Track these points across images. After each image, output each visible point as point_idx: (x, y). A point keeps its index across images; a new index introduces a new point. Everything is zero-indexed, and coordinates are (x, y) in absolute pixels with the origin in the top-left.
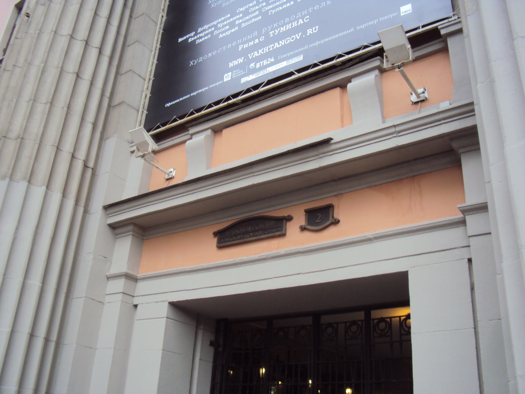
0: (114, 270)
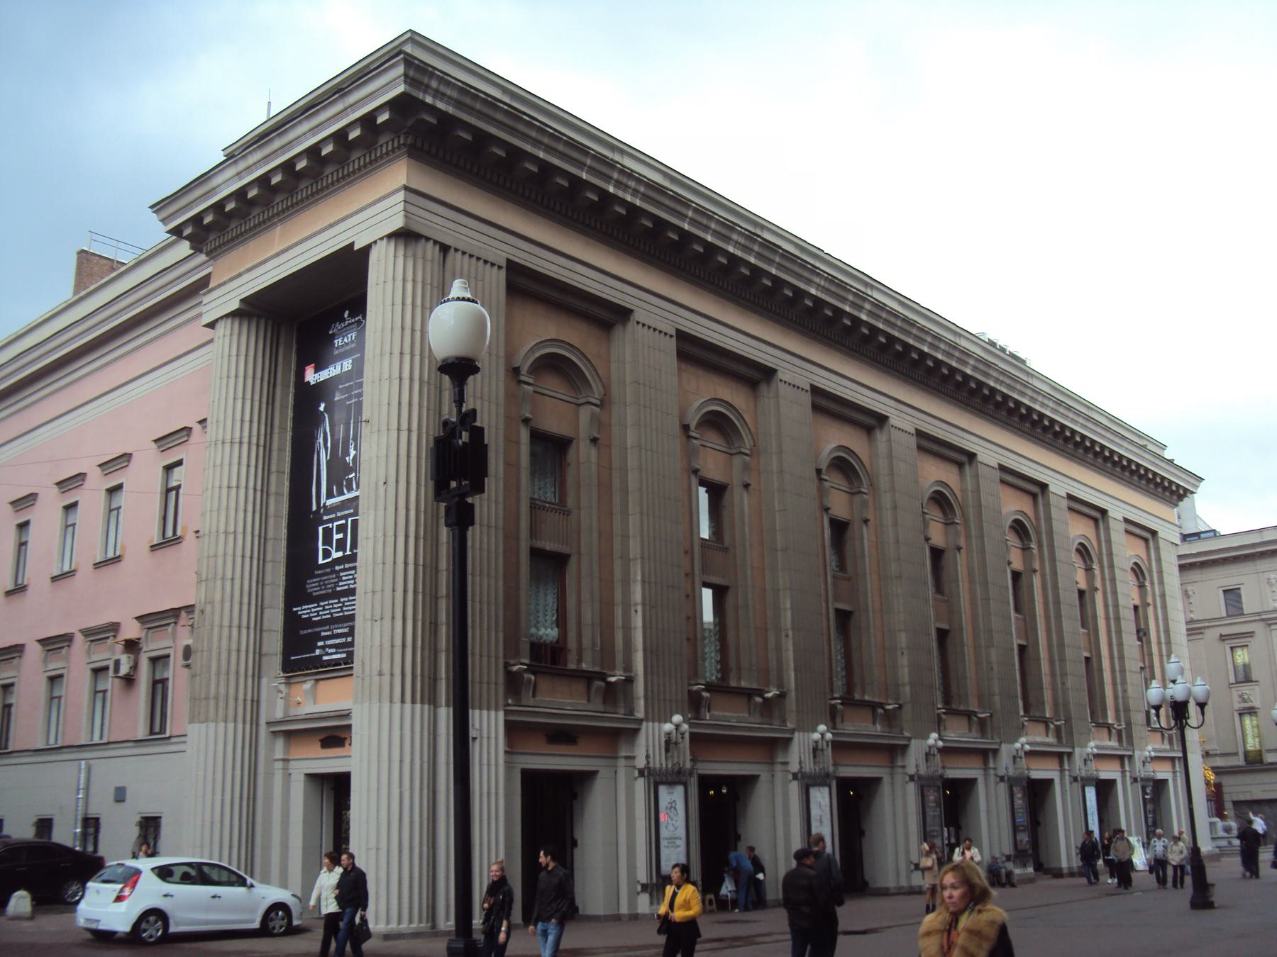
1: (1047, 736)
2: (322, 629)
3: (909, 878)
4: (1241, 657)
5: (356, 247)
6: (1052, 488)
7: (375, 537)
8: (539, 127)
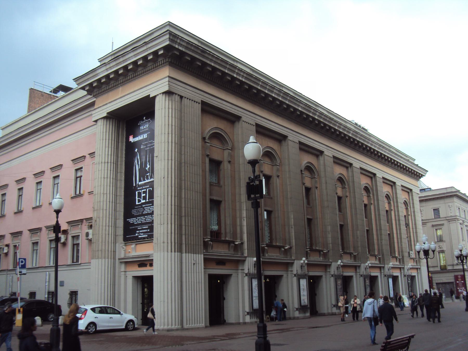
0: (122, 270)
1: (376, 261)
2: (138, 227)
3: (332, 310)
4: (439, 232)
5: (151, 96)
6: (377, 175)
7: (161, 196)
8: (314, 109)
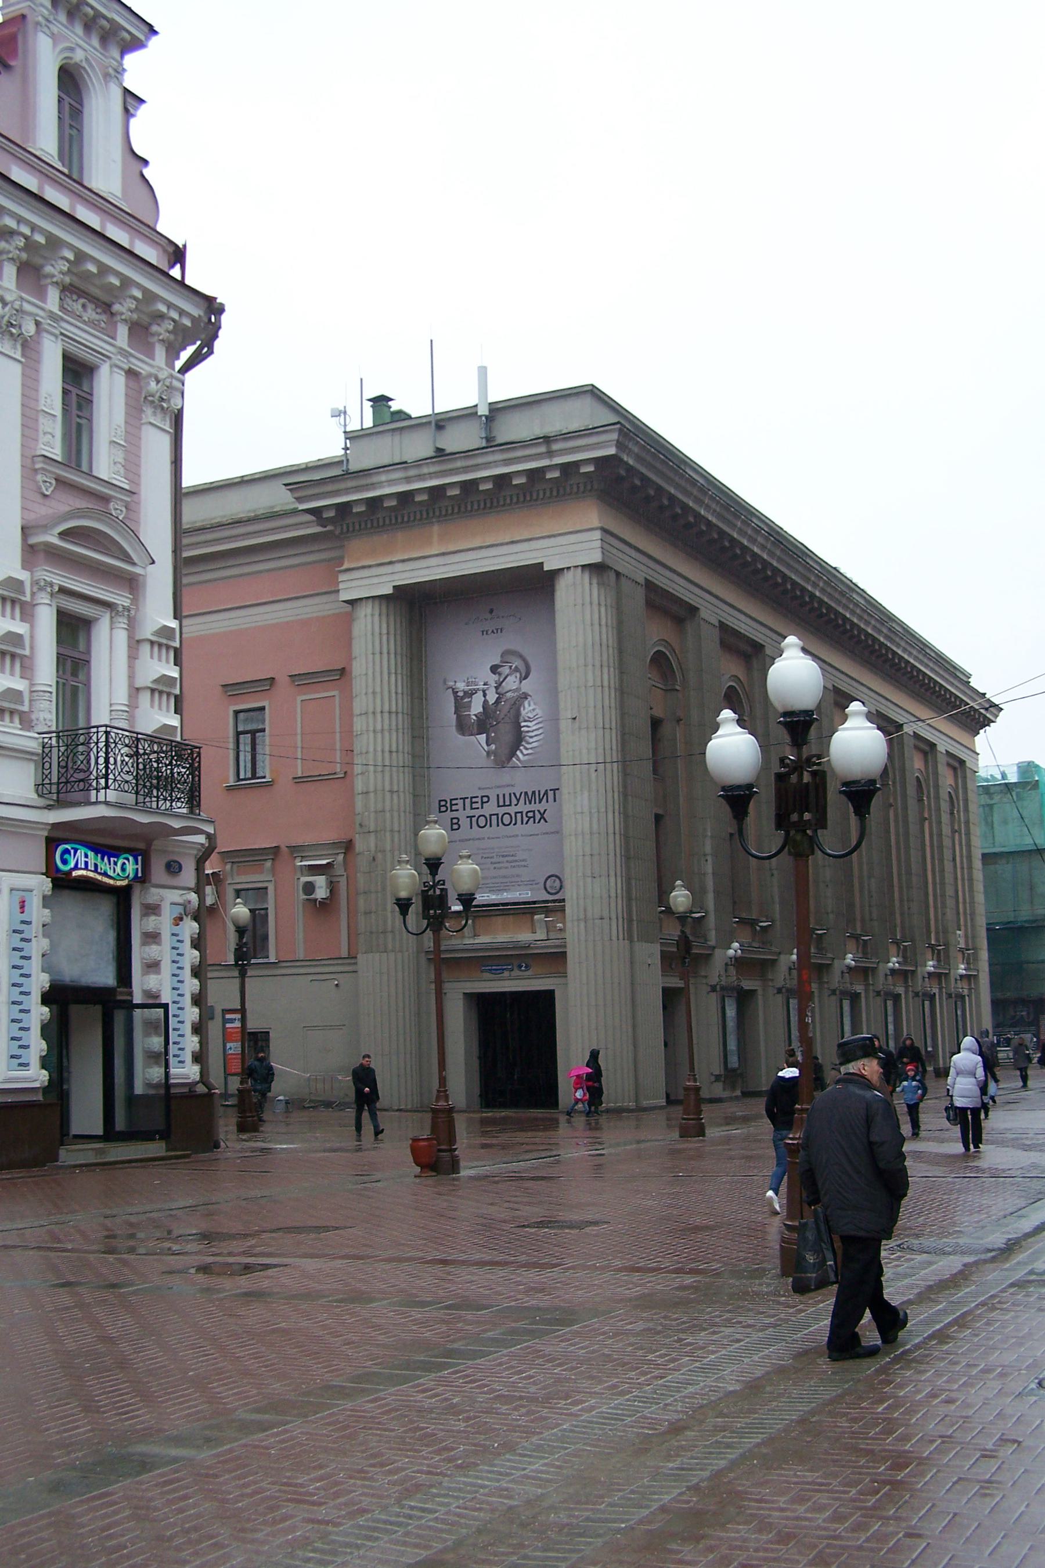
5: (546, 569)
